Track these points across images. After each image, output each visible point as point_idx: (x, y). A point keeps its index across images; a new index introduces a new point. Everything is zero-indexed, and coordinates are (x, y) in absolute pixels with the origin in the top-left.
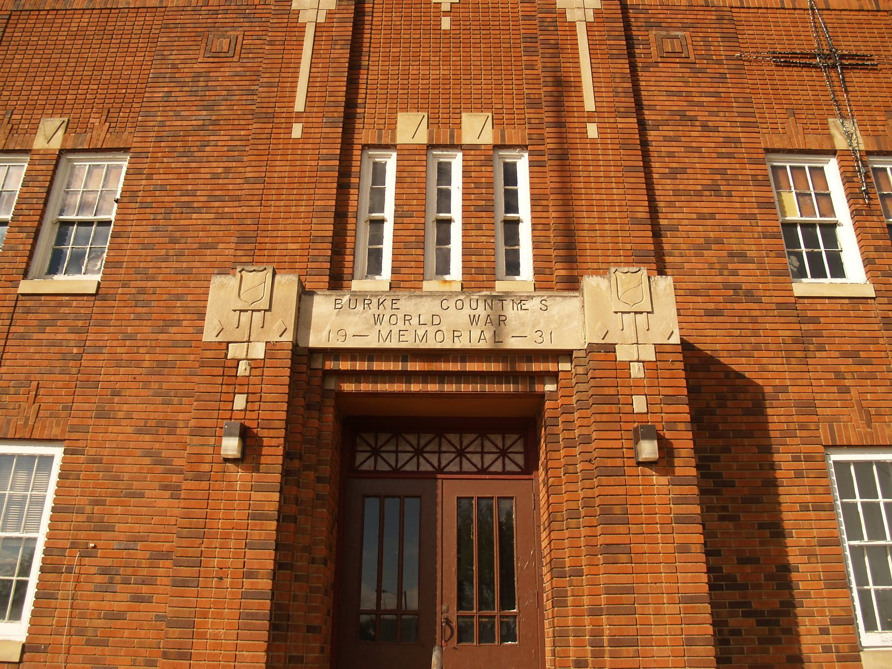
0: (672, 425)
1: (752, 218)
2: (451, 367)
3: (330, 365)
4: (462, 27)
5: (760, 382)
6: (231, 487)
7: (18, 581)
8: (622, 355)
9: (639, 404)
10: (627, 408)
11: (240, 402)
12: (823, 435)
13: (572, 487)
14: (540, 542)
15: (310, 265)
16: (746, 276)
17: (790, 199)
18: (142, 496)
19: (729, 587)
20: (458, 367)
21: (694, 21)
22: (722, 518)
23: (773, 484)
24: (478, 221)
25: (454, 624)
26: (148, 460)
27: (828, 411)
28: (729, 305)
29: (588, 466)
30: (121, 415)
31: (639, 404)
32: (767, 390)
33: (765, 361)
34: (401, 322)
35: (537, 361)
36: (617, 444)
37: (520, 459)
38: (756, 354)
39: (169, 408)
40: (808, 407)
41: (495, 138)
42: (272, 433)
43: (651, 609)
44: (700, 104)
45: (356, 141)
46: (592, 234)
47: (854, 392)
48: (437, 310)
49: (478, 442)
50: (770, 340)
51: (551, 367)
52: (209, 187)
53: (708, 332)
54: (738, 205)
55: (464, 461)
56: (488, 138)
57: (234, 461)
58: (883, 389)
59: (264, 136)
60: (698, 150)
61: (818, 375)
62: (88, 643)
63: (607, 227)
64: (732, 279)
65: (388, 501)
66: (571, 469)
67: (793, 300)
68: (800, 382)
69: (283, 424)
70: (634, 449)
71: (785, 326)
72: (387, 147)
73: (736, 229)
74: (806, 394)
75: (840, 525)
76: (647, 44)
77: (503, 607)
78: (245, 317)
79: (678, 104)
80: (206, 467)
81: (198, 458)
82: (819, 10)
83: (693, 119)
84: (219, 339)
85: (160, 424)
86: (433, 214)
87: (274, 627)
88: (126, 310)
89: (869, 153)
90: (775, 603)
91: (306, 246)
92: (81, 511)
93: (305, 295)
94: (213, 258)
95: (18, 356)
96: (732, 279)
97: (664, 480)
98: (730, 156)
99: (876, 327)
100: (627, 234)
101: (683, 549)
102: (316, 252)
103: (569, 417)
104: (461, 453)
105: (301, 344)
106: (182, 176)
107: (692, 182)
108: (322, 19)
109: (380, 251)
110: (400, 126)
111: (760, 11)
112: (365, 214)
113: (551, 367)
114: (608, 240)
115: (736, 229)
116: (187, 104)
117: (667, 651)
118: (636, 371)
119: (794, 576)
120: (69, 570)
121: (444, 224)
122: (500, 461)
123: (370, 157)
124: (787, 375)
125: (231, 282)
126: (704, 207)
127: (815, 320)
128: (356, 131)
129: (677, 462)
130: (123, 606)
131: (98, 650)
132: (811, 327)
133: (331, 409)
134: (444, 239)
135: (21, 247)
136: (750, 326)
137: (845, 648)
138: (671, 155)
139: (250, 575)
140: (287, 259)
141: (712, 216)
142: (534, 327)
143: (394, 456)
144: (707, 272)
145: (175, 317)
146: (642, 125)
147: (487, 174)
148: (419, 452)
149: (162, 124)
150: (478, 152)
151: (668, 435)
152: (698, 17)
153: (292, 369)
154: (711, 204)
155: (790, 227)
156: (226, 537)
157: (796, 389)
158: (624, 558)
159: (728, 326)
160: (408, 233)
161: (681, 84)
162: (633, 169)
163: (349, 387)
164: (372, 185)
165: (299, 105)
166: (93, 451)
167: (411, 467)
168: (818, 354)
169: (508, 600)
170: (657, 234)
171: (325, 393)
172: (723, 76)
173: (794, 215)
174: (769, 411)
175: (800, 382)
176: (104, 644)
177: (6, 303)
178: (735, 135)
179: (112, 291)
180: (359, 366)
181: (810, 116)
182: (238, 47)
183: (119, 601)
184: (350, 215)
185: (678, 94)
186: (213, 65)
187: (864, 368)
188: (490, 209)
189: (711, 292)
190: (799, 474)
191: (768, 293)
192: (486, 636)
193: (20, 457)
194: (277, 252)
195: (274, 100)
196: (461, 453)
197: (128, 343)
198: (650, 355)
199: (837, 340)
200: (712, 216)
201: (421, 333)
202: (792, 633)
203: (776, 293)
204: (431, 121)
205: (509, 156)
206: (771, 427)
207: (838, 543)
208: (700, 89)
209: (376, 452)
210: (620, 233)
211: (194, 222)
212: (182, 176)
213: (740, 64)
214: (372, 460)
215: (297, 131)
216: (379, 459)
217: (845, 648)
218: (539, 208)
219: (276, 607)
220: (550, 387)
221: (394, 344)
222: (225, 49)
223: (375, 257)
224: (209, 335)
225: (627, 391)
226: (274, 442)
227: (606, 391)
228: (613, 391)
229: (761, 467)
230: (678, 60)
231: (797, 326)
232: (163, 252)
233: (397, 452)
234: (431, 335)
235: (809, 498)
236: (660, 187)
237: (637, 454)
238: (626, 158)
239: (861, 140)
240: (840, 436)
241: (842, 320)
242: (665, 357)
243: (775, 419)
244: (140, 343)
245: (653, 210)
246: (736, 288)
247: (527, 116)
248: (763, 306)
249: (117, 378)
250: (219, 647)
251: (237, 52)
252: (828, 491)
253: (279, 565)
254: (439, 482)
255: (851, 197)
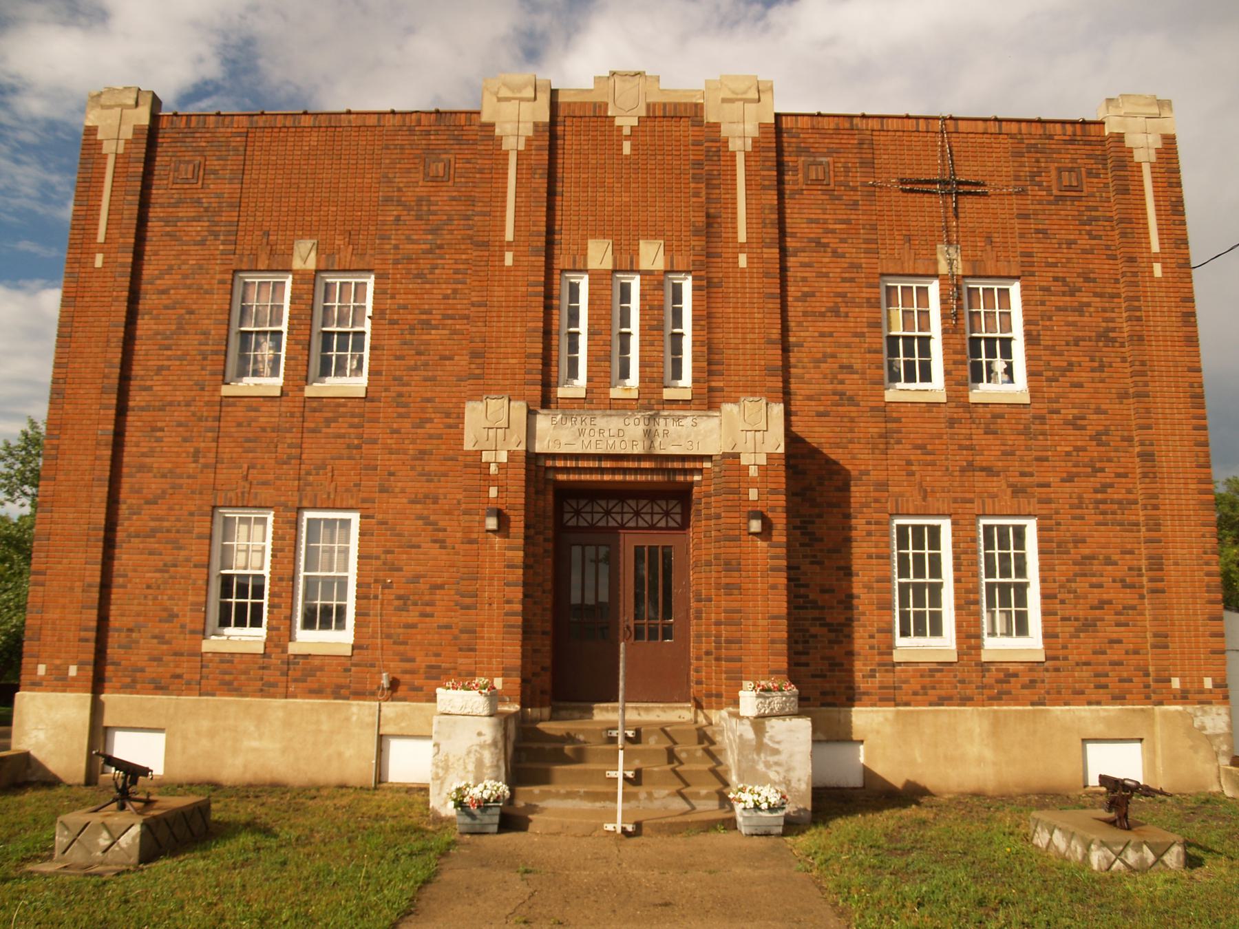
0: (773, 509)
1: (862, 335)
2: (631, 465)
3: (550, 463)
4: (641, 152)
5: (848, 467)
6: (492, 548)
7: (252, 604)
8: (744, 461)
9: (753, 494)
10: (745, 497)
11: (493, 492)
12: (890, 507)
13: (708, 546)
14: (689, 576)
15: (527, 377)
16: (852, 385)
17: (897, 314)
18: (419, 547)
19: (812, 608)
20: (636, 465)
21: (838, 146)
22: (812, 563)
23: (848, 540)
24: (651, 338)
25: (632, 629)
26: (421, 522)
27: (897, 489)
28: (834, 408)
29: (718, 534)
30: (397, 490)
31: (753, 494)
32: (853, 473)
33: (856, 451)
34: (597, 435)
35: (689, 461)
36: (737, 521)
37: (678, 518)
38: (850, 446)
39: (432, 485)
40: (882, 486)
41: (665, 266)
42: (516, 513)
43: (751, 622)
44: (833, 231)
45: (555, 267)
46: (736, 352)
47: (917, 476)
48: (621, 426)
49: (649, 505)
50: (861, 435)
51: (698, 465)
52: (442, 307)
53: (817, 429)
54: (852, 325)
55: (640, 519)
56: (660, 265)
57: (493, 531)
58: (940, 473)
59: (483, 263)
60: (826, 275)
61: (894, 462)
62: (395, 643)
63: (748, 346)
64: (840, 387)
65: (587, 548)
66: (708, 534)
67: (883, 404)
68: (879, 468)
69: (523, 507)
70: (747, 524)
71: (874, 425)
72: (580, 271)
73: (848, 346)
74: (882, 476)
75: (894, 568)
76: (796, 170)
77: (664, 618)
78: (492, 432)
79: (816, 231)
80: (475, 536)
81: (468, 530)
82: (947, 133)
83: (826, 245)
84: (476, 448)
85: (426, 497)
86: (617, 329)
87: (524, 632)
88: (390, 410)
89: (964, 277)
90: (842, 619)
91: (523, 360)
92: (378, 558)
93: (531, 413)
94: (452, 368)
95: (314, 446)
96: (840, 387)
97: (765, 544)
98: (852, 280)
99: (943, 426)
100: (762, 352)
101: (774, 587)
102: (530, 366)
103: (708, 500)
104: (637, 514)
105: (531, 451)
106: (420, 296)
107: (821, 303)
108: (522, 147)
109: (576, 359)
110: (591, 252)
111: (898, 134)
112: (565, 329)
113: (698, 465)
114: (748, 357)
115: (848, 346)
116: (414, 227)
117: (758, 646)
118: (753, 472)
119: (855, 602)
120: (376, 597)
121: (626, 337)
122: (664, 519)
123: (566, 278)
124: (871, 462)
125: (480, 406)
126: (824, 326)
127: (898, 420)
128: (556, 257)
129: (774, 532)
130: (416, 620)
131: (402, 648)
132: (894, 425)
133: (551, 493)
134: (625, 349)
135: (300, 357)
136: (848, 424)
137: (883, 647)
138: (804, 279)
139: (508, 602)
140: (509, 371)
141: (831, 335)
142: (687, 438)
143: (590, 515)
144: (821, 381)
145: (428, 415)
146: (783, 252)
147: (659, 298)
148: (608, 513)
149: (396, 247)
150: (652, 278)
151: (770, 515)
152: (843, 141)
153: (526, 469)
154: (832, 324)
155: (893, 340)
156: (491, 579)
157: (875, 473)
158: (736, 592)
159: (832, 424)
160: (598, 348)
161: (819, 211)
162: (771, 296)
163: (562, 477)
164: (570, 302)
165: (509, 236)
166: (380, 516)
167: (602, 524)
168: (896, 446)
169: (668, 613)
170: (786, 349)
171: (547, 481)
172: (856, 203)
173: (898, 331)
174: (853, 489)
175: (879, 468)
176: (405, 643)
177: (297, 404)
178: (859, 261)
179: (377, 394)
180: (569, 464)
181: (923, 243)
182: (452, 172)
183: (412, 616)
184: (554, 332)
185: (816, 221)
186: (432, 189)
187: (929, 458)
188: (660, 328)
189: (823, 398)
190: (869, 534)
191: (865, 398)
192: (653, 635)
193: (326, 520)
194: (501, 366)
195: (487, 229)
196: (637, 514)
197: (395, 436)
198: (763, 460)
199: (912, 436)
200: (831, 335)
201: (611, 442)
202: (850, 637)
203: (871, 399)
204: (615, 247)
205: (676, 278)
206: (852, 500)
207: (889, 580)
208: (835, 217)
209: (578, 513)
210: (757, 351)
211: (433, 337)
212: (420, 296)
213: (872, 191)
214: (575, 519)
215: (509, 259)
216: (580, 518)
217: (883, 647)
218: (698, 328)
219: (525, 620)
220: (697, 478)
221: (592, 450)
222: (441, 173)
223: (573, 364)
224: (468, 446)
225: (745, 485)
226: (518, 518)
227: (732, 485)
228: (736, 485)
229: (843, 529)
230: (820, 187)
231: (883, 425)
232: (412, 362)
233: (592, 512)
234: (617, 444)
235: (874, 550)
236: (793, 309)
237: (748, 528)
238: (767, 285)
239: (960, 266)
240: (902, 507)
241: (918, 420)
242: (773, 462)
243: (858, 494)
244: (405, 436)
245: (785, 330)
246: (842, 394)
247: (693, 243)
248: (861, 409)
249: (391, 463)
250: (493, 644)
251: (452, 176)
252: (888, 545)
253: (525, 596)
254: (622, 535)
255: (945, 317)
